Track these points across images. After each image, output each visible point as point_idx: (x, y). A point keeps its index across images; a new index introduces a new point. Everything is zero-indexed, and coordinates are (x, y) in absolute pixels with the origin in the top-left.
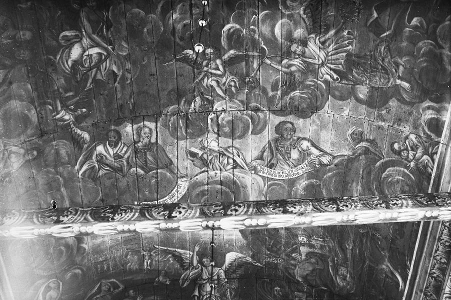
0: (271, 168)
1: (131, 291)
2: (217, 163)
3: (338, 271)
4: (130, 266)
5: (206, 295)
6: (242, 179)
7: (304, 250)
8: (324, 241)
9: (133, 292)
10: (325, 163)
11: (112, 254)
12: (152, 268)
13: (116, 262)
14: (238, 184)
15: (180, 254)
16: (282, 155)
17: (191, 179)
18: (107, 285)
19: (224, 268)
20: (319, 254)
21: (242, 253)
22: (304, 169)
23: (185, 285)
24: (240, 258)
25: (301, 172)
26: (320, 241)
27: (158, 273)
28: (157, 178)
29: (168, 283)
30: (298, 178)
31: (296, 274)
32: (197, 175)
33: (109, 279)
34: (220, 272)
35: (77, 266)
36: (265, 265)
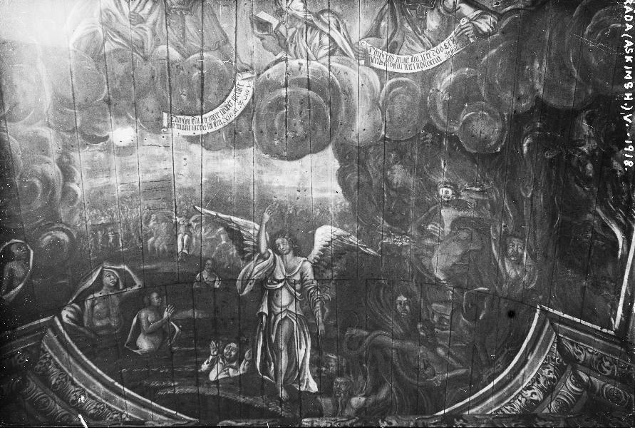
0: (392, 52)
1: (155, 295)
2: (302, 44)
3: (506, 249)
4: (153, 242)
5: (281, 313)
6: (343, 76)
7: (448, 214)
8: (482, 192)
9: (158, 298)
10: (485, 30)
11: (123, 213)
12: (191, 253)
13: (129, 230)
14: (337, 86)
15: (238, 226)
16: (411, 23)
17: (258, 75)
18: (114, 275)
19: (311, 257)
20: (473, 218)
21: (342, 228)
22: (449, 50)
23: (245, 292)
24: (339, 237)
25: (443, 57)
26: (476, 192)
27: (202, 262)
28: (201, 69)
29: (216, 285)
30: (436, 70)
31: (434, 265)
32: (268, 68)
33: (118, 264)
34: (305, 266)
35: (61, 226)
36: (381, 252)
